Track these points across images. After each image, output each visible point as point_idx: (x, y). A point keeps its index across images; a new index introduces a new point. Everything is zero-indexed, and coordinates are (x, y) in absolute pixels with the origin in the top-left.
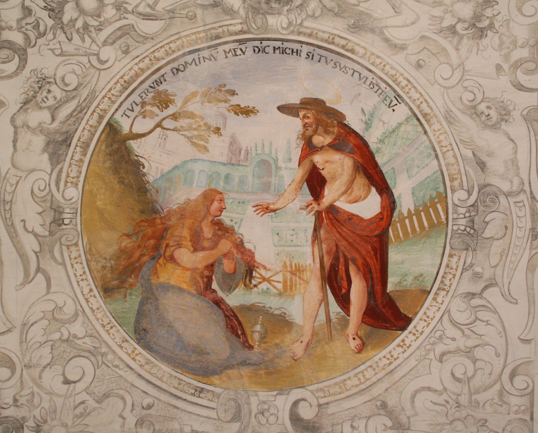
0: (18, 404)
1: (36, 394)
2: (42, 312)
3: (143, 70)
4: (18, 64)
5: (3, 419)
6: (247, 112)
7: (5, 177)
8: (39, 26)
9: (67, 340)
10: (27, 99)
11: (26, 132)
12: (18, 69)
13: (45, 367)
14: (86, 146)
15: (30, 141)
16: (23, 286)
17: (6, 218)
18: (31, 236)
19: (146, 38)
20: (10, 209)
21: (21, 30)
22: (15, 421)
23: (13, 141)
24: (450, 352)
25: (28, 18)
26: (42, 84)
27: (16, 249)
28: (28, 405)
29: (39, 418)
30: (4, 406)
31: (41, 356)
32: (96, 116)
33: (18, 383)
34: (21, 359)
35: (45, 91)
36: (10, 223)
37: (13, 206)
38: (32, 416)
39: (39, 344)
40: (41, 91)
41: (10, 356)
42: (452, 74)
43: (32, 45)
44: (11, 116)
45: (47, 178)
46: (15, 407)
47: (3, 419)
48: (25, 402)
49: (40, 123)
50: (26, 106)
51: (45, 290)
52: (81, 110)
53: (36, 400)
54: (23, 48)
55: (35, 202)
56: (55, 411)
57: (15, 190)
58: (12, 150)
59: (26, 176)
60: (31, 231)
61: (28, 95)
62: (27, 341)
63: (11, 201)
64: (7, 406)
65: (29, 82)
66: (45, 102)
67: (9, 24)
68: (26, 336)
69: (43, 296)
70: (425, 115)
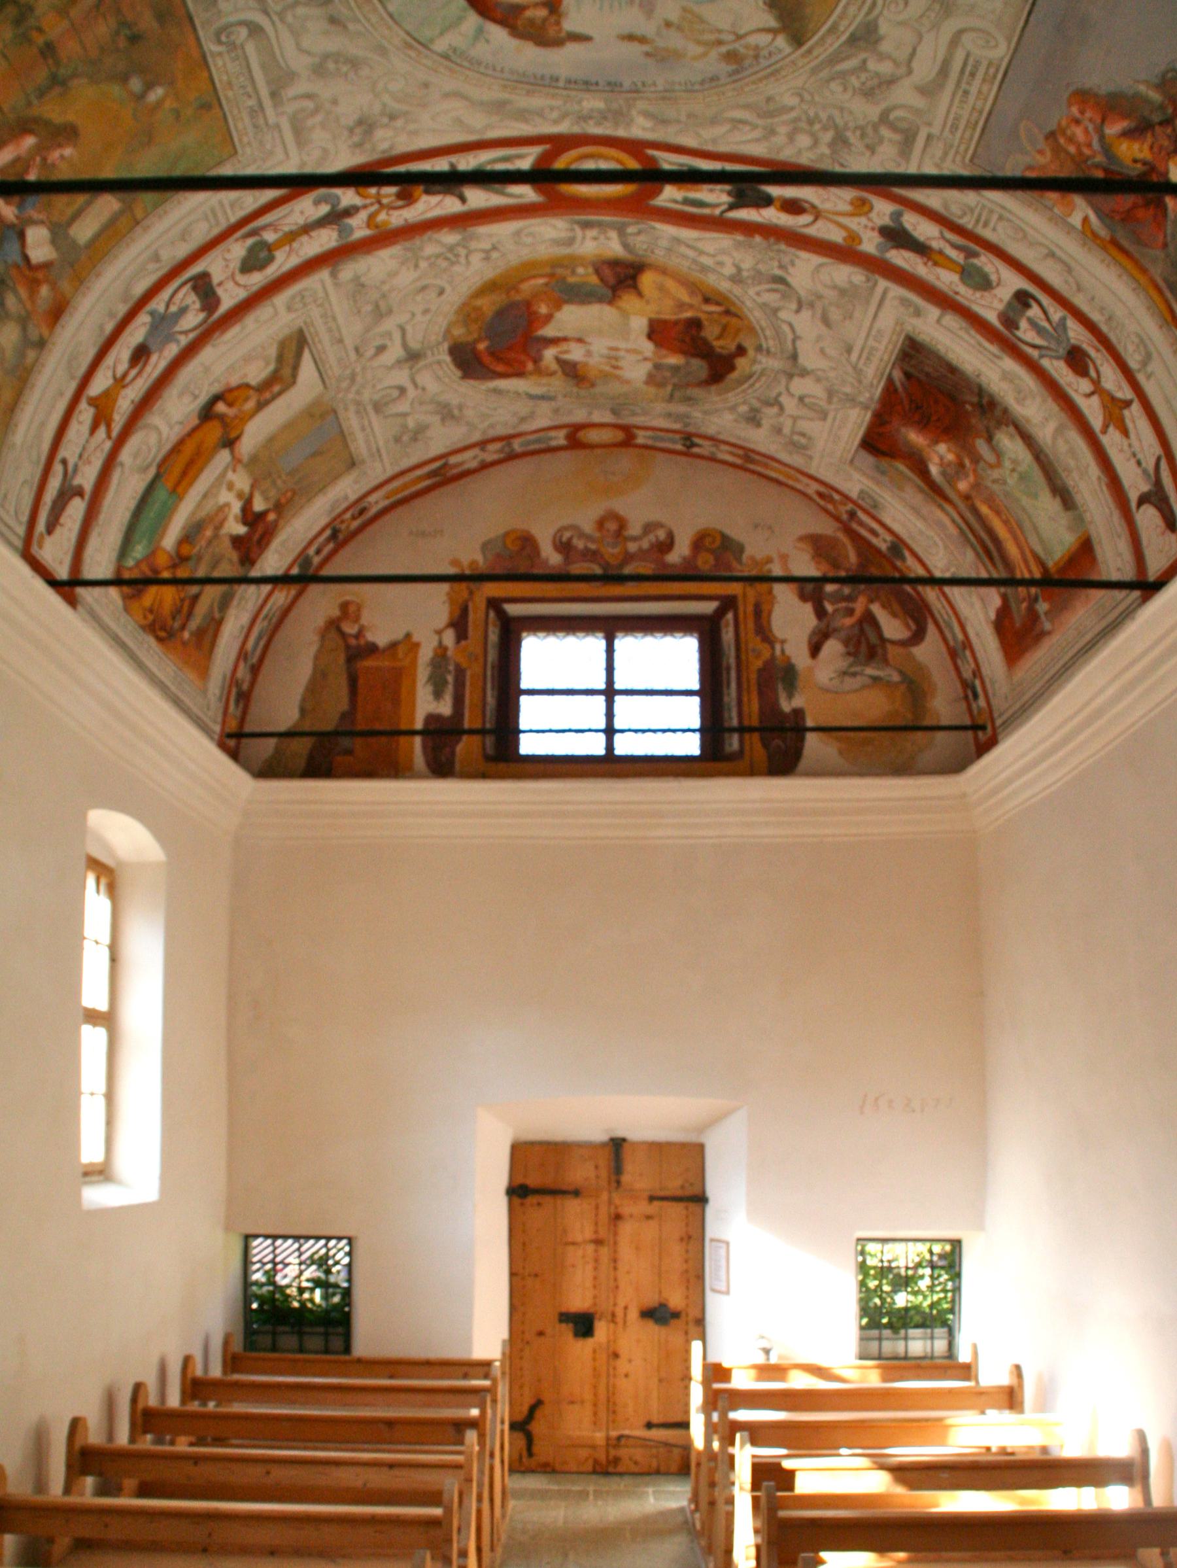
3: (754, 83)
6: (631, 38)
14: (833, 29)
19: (747, 107)
32: (815, 53)
45: (885, 12)
52: (833, 60)
58: (918, 49)
70: (410, 47)
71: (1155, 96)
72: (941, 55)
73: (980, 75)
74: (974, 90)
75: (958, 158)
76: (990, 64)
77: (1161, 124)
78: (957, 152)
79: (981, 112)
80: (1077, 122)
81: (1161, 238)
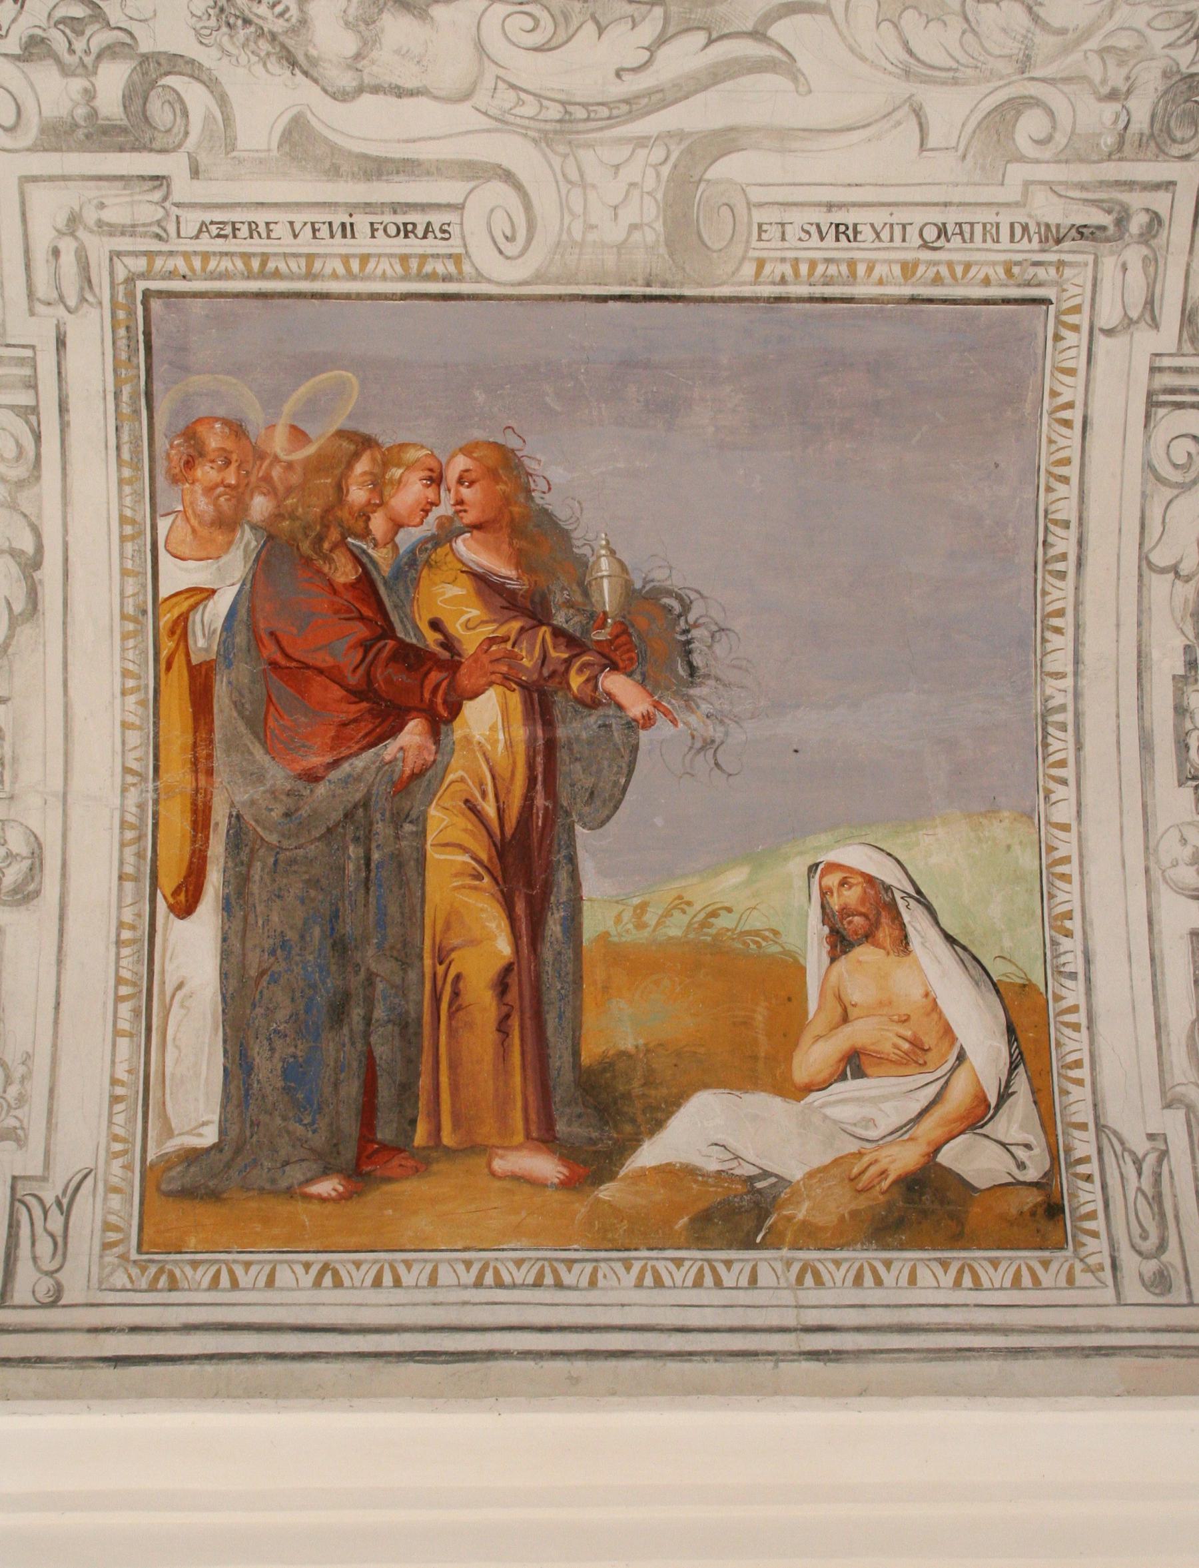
0: (1125, 89)
1: (1110, 42)
2: (878, 25)
4: (186, 79)
5: (1157, 126)
7: (496, 119)
8: (73, 19)
10: (280, 58)
11: (373, 62)
12: (198, 79)
13: (1036, 19)
15: (397, 52)
16: (799, 76)
17: (609, 118)
18: (664, 52)
20: (585, 105)
21: (90, 67)
22: (1171, 95)
23: (399, 96)
25: (55, 46)
26: (237, 17)
27: (696, 92)
28: (1132, 63)
29: (1178, 33)
30: (1121, 125)
31: (1004, 30)
33: (1066, 88)
34: (1001, 83)
35: (255, 10)
36: (625, 108)
37: (578, 100)
38: (1167, 51)
39: (969, 36)
40: (255, 20)
41: (985, 113)
42: (489, 218)
43: (128, 40)
44: (328, 99)
46: (1132, 97)
47: (1157, 126)
48: (1124, 71)
49: (347, 23)
50: (301, 59)
51: (818, 17)
53: (1125, 41)
54: (141, 64)
55: (566, 42)
57: (534, 95)
58: (423, 101)
59: (496, 63)
60: (648, 54)
61: (268, 54)
62: (955, 66)
63: (563, 103)
64: (1123, 118)
65: (234, 51)
66: (287, 9)
67: (77, 97)
68: (940, 69)
69: (835, 24)
71: (607, 596)
72: (425, 152)
73: (414, 246)
74: (362, 243)
75: (140, 264)
76: (457, 259)
77: (558, 632)
78: (150, 255)
79: (310, 276)
80: (436, 479)
81: (316, 761)
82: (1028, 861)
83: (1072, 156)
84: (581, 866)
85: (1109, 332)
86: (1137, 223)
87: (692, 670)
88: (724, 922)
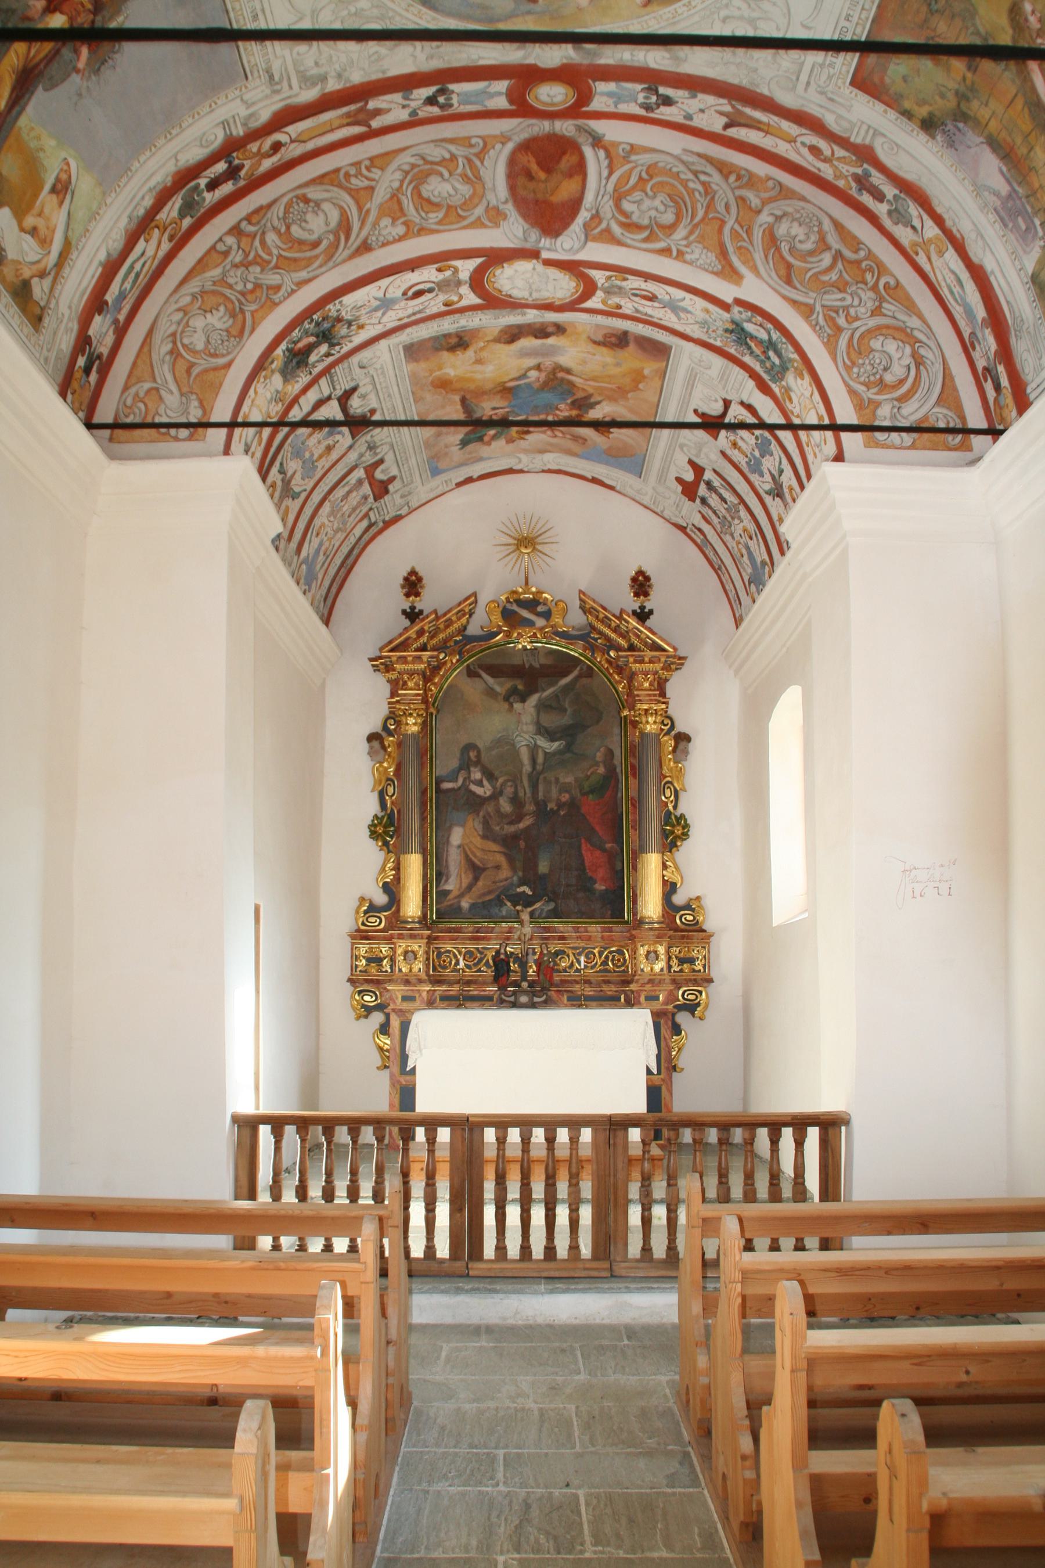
9: (355, 14)
24: (733, 17)
53: (334, 59)
56: (352, 62)
82: (94, 207)
83: (295, 63)
84: (606, 1295)
85: (242, 100)
86: (278, 87)
87: (99, 69)
88: (41, 155)
